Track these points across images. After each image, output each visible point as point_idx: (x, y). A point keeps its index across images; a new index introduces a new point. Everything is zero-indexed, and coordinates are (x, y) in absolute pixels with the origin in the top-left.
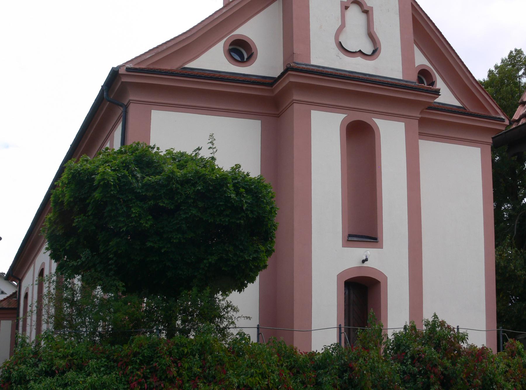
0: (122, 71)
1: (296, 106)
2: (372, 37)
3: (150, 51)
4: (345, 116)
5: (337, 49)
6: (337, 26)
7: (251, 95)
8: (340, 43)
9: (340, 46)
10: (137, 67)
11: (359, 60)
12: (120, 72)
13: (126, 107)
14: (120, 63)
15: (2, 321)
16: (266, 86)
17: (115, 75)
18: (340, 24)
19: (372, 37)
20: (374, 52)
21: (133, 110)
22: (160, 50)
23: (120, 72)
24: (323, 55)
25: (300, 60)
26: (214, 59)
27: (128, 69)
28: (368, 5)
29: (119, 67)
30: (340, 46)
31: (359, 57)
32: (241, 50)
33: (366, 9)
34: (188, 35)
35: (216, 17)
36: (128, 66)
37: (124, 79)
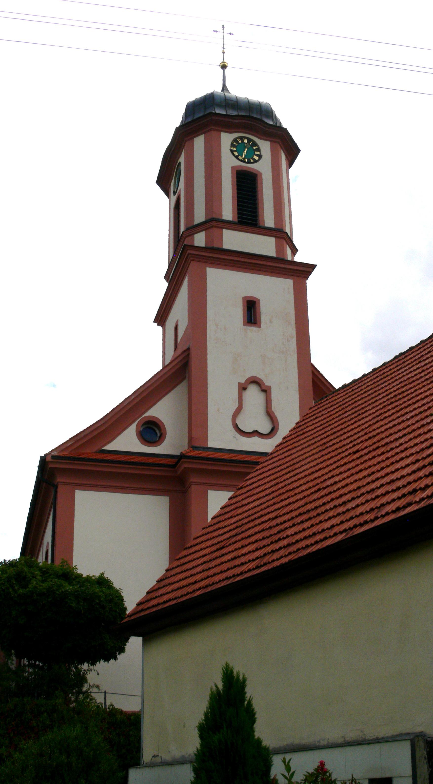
0: (49, 459)
1: (194, 487)
2: (270, 415)
3: (71, 439)
4: (230, 494)
5: (233, 430)
6: (235, 408)
7: (150, 475)
8: (237, 424)
9: (236, 427)
10: (61, 454)
11: (256, 439)
12: (47, 460)
13: (56, 487)
14: (47, 452)
15: (77, 491)
16: (128, 465)
17: (44, 461)
18: (237, 405)
19: (270, 415)
20: (273, 430)
21: (61, 489)
22: (78, 438)
23: (47, 460)
24: (220, 437)
25: (197, 444)
26: (128, 441)
27: (54, 457)
28: (266, 384)
29: (46, 455)
30: (236, 427)
31: (256, 437)
32: (152, 431)
33: (264, 388)
34: (102, 422)
35: (125, 404)
36: (53, 454)
37: (51, 466)
